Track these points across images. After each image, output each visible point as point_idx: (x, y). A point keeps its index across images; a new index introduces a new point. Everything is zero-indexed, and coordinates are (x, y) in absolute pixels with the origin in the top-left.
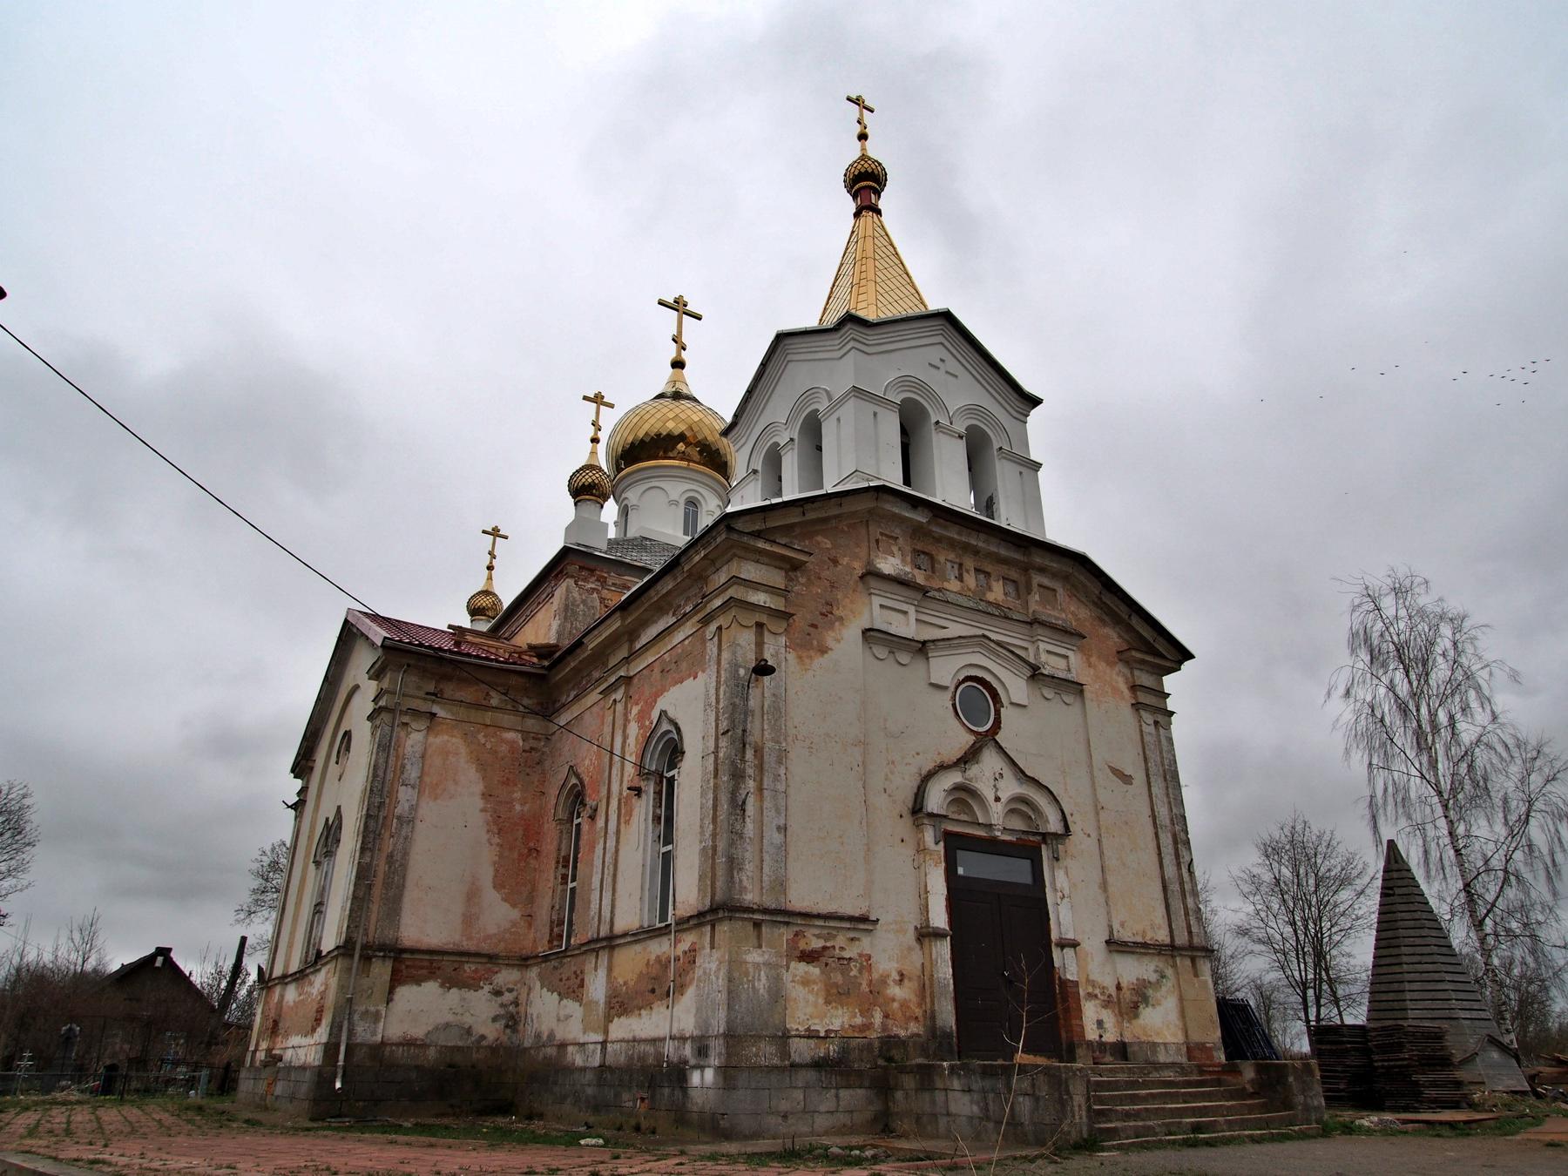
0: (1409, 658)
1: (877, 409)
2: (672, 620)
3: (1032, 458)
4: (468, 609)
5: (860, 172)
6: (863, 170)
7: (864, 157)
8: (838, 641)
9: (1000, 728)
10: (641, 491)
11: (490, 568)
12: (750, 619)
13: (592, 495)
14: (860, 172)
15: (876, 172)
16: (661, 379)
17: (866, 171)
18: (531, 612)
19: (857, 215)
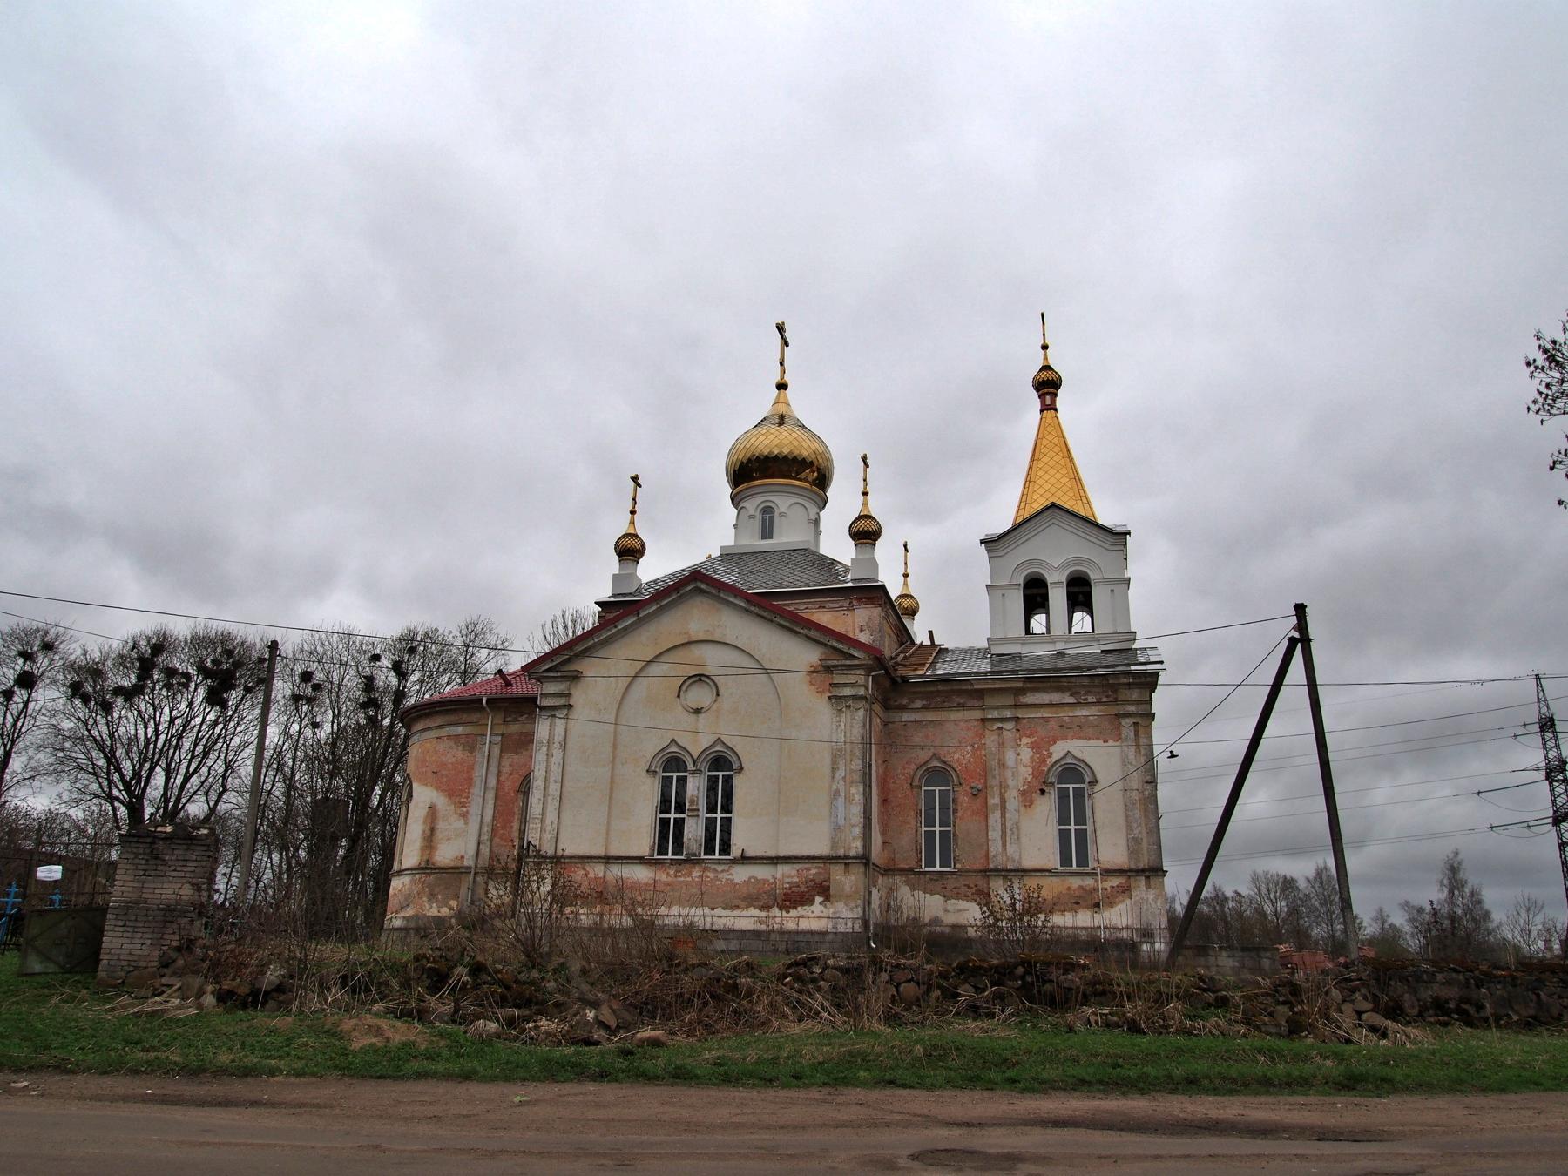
0: (144, 882)
1: (1112, 587)
2: (1072, 700)
3: (821, 552)
4: (615, 548)
5: (1043, 380)
6: (1046, 379)
7: (1046, 368)
8: (437, 630)
9: (412, 796)
10: (757, 504)
11: (633, 512)
12: (1129, 721)
13: (871, 539)
14: (1043, 380)
15: (1050, 378)
16: (764, 402)
17: (1048, 379)
18: (807, 608)
19: (1042, 411)
